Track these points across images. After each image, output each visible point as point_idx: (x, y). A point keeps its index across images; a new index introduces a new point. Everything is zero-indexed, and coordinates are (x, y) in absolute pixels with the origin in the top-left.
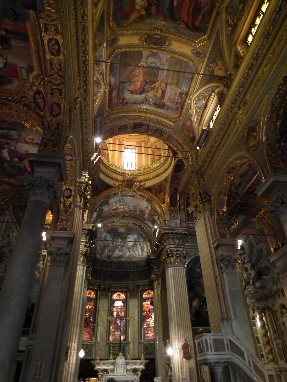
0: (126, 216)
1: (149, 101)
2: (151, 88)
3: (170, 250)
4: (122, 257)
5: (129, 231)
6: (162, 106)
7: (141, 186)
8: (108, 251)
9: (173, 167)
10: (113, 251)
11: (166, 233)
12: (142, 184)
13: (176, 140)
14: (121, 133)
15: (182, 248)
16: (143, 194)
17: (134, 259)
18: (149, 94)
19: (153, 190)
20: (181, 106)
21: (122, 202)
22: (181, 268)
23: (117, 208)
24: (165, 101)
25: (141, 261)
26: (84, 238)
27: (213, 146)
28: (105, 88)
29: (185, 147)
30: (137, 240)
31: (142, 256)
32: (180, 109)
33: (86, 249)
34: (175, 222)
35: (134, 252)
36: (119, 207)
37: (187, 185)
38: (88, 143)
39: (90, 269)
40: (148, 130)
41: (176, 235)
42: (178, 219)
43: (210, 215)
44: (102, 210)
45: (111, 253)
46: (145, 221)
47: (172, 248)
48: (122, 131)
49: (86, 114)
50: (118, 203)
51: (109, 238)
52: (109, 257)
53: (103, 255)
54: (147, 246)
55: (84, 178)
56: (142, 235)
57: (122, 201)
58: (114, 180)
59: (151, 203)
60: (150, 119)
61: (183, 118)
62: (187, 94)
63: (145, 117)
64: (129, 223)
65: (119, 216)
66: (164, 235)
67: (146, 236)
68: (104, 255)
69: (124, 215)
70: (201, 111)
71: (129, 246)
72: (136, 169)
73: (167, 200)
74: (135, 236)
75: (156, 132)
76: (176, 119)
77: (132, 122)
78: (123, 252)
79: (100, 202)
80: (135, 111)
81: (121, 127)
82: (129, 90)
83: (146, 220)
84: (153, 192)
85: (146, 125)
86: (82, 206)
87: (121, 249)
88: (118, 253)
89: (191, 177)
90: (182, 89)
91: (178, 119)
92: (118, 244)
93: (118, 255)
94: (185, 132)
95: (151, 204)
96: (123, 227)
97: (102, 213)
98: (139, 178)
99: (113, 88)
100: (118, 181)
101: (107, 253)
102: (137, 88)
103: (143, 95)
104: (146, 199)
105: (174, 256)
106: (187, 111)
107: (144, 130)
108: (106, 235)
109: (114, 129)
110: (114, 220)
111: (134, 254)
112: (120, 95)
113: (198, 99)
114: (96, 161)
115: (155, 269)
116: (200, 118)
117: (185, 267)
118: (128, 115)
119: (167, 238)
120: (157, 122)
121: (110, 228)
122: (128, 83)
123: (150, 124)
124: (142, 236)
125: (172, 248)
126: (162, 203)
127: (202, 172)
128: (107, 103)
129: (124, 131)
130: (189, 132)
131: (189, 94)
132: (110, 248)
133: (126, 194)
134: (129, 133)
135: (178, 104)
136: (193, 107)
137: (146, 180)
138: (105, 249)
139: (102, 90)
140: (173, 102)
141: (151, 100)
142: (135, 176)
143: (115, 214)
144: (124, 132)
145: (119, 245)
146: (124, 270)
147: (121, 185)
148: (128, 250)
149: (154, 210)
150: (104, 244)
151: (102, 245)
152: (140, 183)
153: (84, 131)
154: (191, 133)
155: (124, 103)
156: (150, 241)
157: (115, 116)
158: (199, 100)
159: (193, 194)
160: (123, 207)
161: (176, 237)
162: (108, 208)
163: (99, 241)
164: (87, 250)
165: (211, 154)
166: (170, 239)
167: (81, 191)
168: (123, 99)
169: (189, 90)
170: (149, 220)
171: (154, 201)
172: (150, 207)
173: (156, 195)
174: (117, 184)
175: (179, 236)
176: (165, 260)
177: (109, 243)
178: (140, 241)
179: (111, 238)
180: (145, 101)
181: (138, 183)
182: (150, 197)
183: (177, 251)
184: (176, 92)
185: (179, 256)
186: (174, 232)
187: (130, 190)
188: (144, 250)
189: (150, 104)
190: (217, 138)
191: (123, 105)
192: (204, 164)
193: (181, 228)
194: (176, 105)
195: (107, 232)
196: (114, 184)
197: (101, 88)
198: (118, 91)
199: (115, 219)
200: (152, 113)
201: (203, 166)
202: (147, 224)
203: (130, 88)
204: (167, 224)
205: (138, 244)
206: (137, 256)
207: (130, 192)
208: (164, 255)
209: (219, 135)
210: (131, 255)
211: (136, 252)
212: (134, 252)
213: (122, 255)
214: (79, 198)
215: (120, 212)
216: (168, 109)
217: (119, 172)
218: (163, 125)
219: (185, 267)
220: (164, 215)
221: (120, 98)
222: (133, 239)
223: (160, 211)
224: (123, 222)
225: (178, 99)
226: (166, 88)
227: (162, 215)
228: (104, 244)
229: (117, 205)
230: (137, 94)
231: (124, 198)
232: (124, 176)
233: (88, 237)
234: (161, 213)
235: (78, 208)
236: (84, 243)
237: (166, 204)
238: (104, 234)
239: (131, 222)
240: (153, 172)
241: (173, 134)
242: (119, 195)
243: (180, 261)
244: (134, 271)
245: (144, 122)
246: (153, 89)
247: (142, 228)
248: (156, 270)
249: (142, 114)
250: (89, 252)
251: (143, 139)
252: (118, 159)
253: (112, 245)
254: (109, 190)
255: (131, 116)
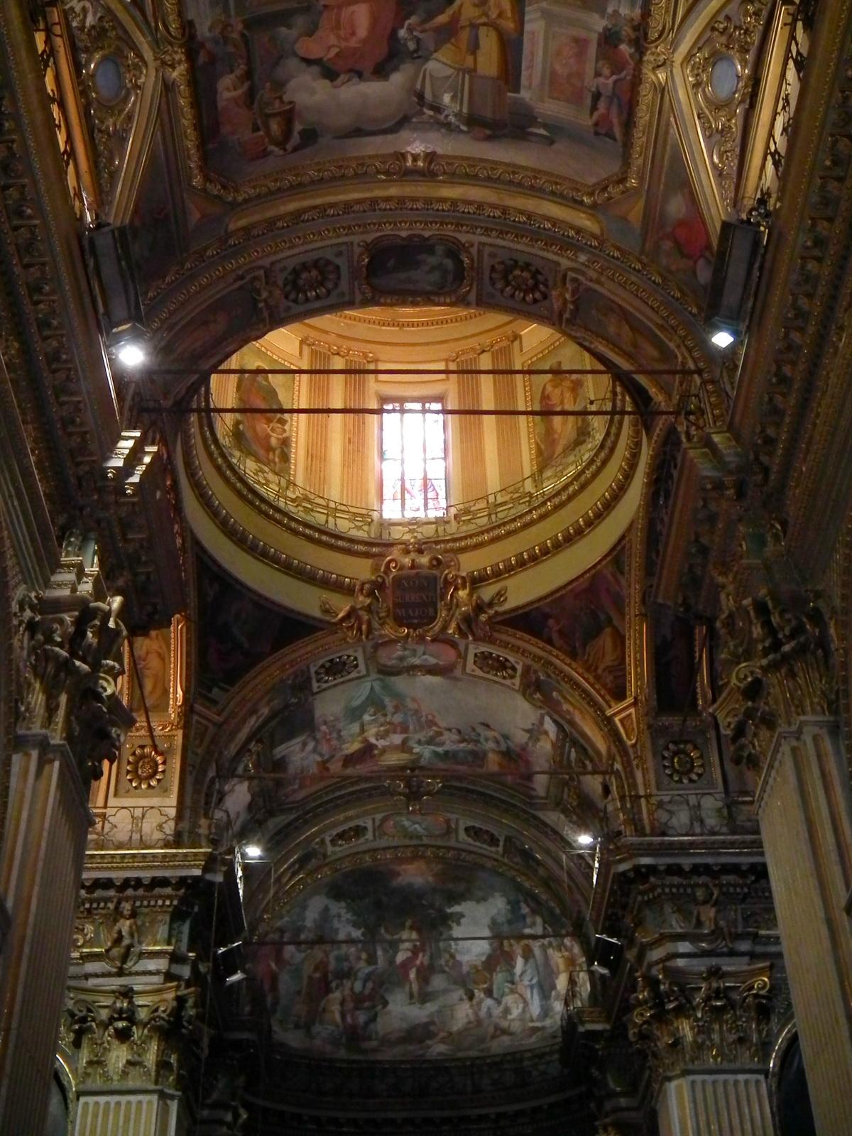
0: (428, 793)
1: (437, 109)
2: (438, 30)
3: (675, 975)
4: (431, 1035)
5: (460, 879)
6: (513, 125)
7: (480, 608)
8: (342, 1003)
9: (648, 475)
10: (374, 999)
11: (642, 874)
12: (487, 593)
13: (625, 316)
14: (301, 308)
15: (742, 954)
16: (496, 651)
17: (500, 1045)
18: (431, 65)
19: (551, 622)
20: (620, 111)
21: (390, 709)
22: (741, 1077)
23: (368, 749)
24: (525, 94)
25: (539, 1056)
26: (162, 931)
27: (800, 314)
28: (164, 63)
29: (672, 345)
30: (506, 929)
31: (548, 1022)
32: (617, 131)
33: (170, 995)
34: (693, 800)
35: (499, 1002)
36: (381, 743)
37: (698, 571)
38: (68, 379)
39: (236, 1116)
40: (459, 275)
41: (701, 880)
42: (712, 784)
43: (823, 732)
44: (280, 765)
45: (362, 1018)
46: (540, 814)
47: (681, 962)
48: (307, 300)
49: (20, 214)
50: (367, 718)
51: (346, 929)
52: (354, 1036)
53: (317, 1028)
54: (571, 962)
55: (71, 577)
56: (535, 898)
57: (389, 703)
58: (325, 583)
59: (551, 698)
60: (461, 208)
61: (641, 179)
62: (640, 42)
63: (428, 201)
64: (449, 831)
65: (389, 793)
66: (632, 881)
67: (547, 899)
68: (322, 1031)
69: (412, 784)
70: (736, 124)
71: (465, 969)
72: (453, 511)
73: (638, 674)
74: (497, 905)
75: (508, 283)
76: (605, 189)
77: (356, 239)
78: (431, 1007)
79: (252, 722)
80: (363, 175)
81: (296, 272)
82: (308, 62)
83: (543, 807)
84: (555, 636)
85: (440, 249)
86: (57, 739)
87: (420, 988)
88: (401, 1010)
89: (712, 519)
90: (610, 10)
91: (615, 191)
92: (400, 957)
93: (405, 1026)
94: (664, 261)
95: (550, 705)
96: (423, 857)
97: (279, 784)
98: (470, 563)
99: (213, 59)
100: (349, 591)
101: (343, 1016)
102: (353, 43)
103: (397, 79)
104: (517, 681)
105: (694, 1009)
106: (661, 134)
107: (435, 277)
108: (326, 909)
109: (259, 293)
110: (358, 817)
111: (497, 1011)
112: (265, 93)
113: (710, 56)
114: (135, 479)
115: (614, 1095)
116: (735, 164)
117: (766, 1073)
118: (332, 205)
119: (648, 903)
120: (504, 223)
121: (347, 866)
122: (300, 21)
123: (463, 238)
124: (538, 907)
125: (681, 962)
126: (610, 691)
127: (766, 478)
128: (190, 143)
129: (318, 297)
130: (689, 257)
131: (653, 35)
132: (358, 986)
133: (401, 659)
134: (351, 304)
135: (602, 105)
136: (685, 108)
137: (510, 569)
138: (328, 990)
139: (149, 79)
140: (576, 98)
141: (447, 98)
142: (446, 551)
143: (359, 783)
144: (317, 304)
145: (406, 965)
146: (447, 1113)
147: (368, 609)
148: (460, 992)
149: (575, 743)
150: (321, 966)
151: (308, 969)
152: (473, 590)
153: (28, 308)
154: (701, 262)
155: (295, 139)
156: (578, 932)
157: (256, 218)
158: (716, 58)
159: (731, 616)
160: (404, 742)
161: (700, 894)
162: (315, 750)
163: (289, 949)
164: (181, 1000)
165: (801, 367)
166: (668, 909)
167: (49, 657)
168: (289, 117)
169: (646, 14)
170: (559, 805)
171: (565, 687)
172: (549, 725)
173: (573, 655)
174: (342, 606)
175: (720, 886)
176: (643, 1037)
177: (347, 958)
178: (527, 931)
179: (356, 925)
180: (417, 112)
181: (462, 594)
182: (536, 666)
183: (715, 973)
184: (582, 34)
185: (724, 1004)
186: (686, 862)
187: (422, 638)
188: (553, 987)
189: (447, 125)
190: (811, 266)
191: (289, 147)
192: (771, 431)
193: (733, 833)
194: (594, 108)
195: (329, 895)
196: (326, 611)
197: (136, 66)
198: (248, 75)
199: (366, 813)
200: (468, 173)
201: (770, 442)
202: (556, 832)
203: (312, 47)
204: (645, 815)
205: (518, 949)
206: (516, 1027)
207: (421, 649)
208: (640, 1003)
209: (819, 242)
210: (479, 1022)
211: (509, 1000)
212: (499, 1002)
213: (427, 1025)
214: (37, 699)
215: (390, 769)
216: (551, 142)
217: (352, 541)
218: (535, 236)
219: (766, 1073)
220: (627, 764)
221: (269, 111)
222: (487, 921)
223: (601, 745)
224: (416, 824)
225: (598, 74)
226: (521, 23)
227: (618, 766)
228: (321, 966)
229: (363, 730)
230: (360, 75)
231: (400, 683)
232: (382, 555)
233: (186, 929)
234: (611, 758)
235: (35, 754)
236: (162, 964)
237: (630, 700)
238: (315, 906)
239: (462, 826)
240: (543, 517)
241: (598, 282)
242: (362, 667)
243: (732, 1037)
244: (499, 1115)
245: (427, 234)
246: (448, 33)
247: (527, 855)
248: (623, 1102)
249: (408, 190)
250: (192, 1012)
251: (486, 340)
252: (345, 464)
253: (364, 969)
254: (300, 643)
255: (348, 207)
